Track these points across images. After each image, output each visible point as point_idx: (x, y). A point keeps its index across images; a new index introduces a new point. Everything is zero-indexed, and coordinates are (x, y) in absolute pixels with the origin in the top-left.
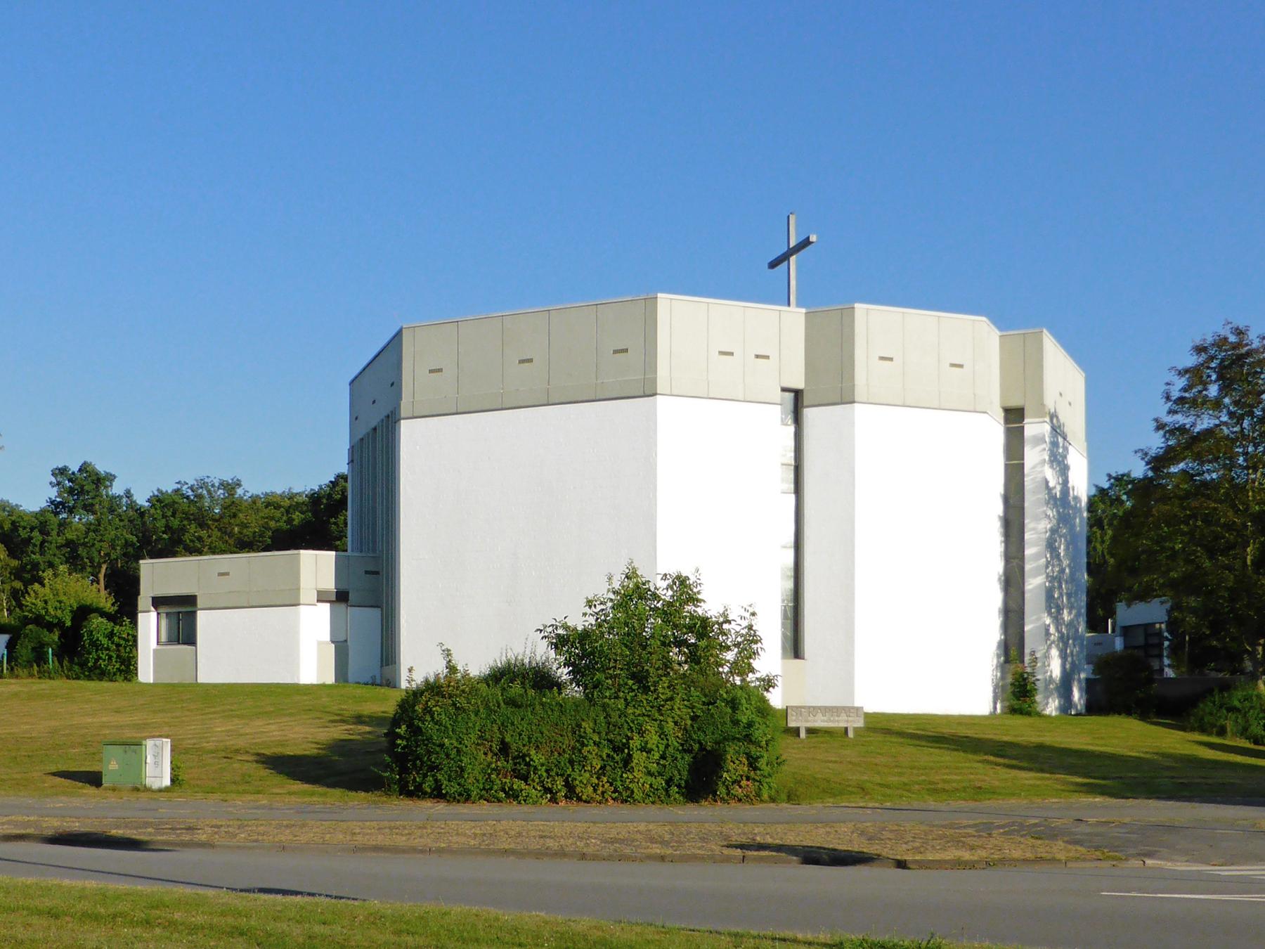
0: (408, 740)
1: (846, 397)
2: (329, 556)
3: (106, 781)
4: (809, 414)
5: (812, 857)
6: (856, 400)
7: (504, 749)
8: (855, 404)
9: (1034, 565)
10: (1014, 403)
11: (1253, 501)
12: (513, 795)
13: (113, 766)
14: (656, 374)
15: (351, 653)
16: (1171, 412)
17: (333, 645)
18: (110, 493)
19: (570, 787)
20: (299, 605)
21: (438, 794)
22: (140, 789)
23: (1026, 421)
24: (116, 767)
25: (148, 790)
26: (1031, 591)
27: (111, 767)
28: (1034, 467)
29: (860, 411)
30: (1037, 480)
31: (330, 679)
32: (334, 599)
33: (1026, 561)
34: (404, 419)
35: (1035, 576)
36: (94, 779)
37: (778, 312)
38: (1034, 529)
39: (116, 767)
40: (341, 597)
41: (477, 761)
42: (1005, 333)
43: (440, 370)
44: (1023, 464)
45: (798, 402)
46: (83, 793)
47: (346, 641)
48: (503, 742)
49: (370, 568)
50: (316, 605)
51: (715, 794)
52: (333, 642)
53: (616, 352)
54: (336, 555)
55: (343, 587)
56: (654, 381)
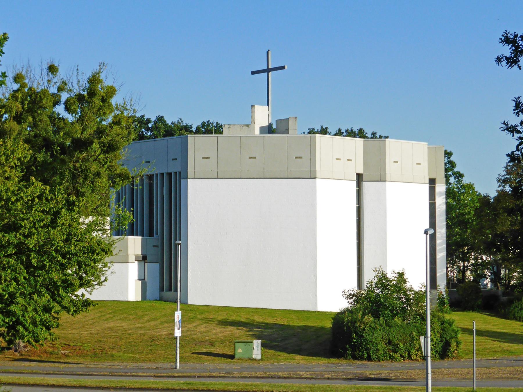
0: (357, 340)
1: (382, 179)
3: (236, 357)
4: (366, 186)
6: (387, 180)
7: (389, 343)
8: (387, 182)
9: (440, 248)
10: (433, 177)
12: (392, 358)
13: (240, 351)
14: (316, 169)
16: (499, 186)
17: (141, 282)
19: (410, 355)
20: (128, 263)
21: (369, 359)
22: (252, 359)
23: (437, 185)
24: (241, 351)
25: (256, 360)
26: (440, 258)
27: (238, 351)
29: (388, 185)
30: (441, 211)
31: (139, 299)
32: (141, 259)
34: (190, 179)
36: (232, 357)
37: (354, 141)
38: (440, 232)
39: (241, 351)
40: (144, 258)
41: (382, 347)
42: (429, 146)
45: (359, 178)
47: (144, 279)
48: (389, 339)
49: (155, 244)
50: (134, 263)
51: (448, 356)
53: (296, 158)
54: (142, 239)
55: (145, 254)
56: (315, 172)
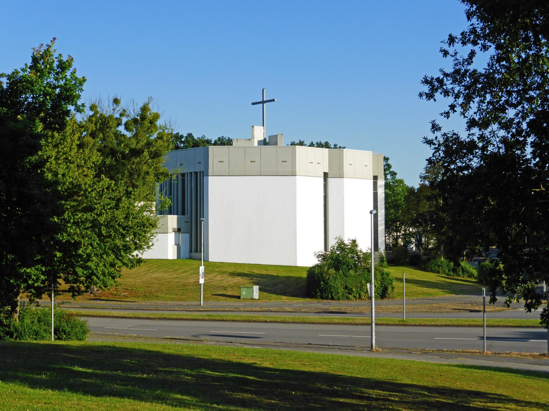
1: (341, 176)
2: (175, 217)
3: (242, 297)
4: (330, 181)
5: (471, 311)
10: (376, 175)
11: (523, 243)
12: (348, 298)
13: (244, 293)
15: (181, 249)
17: (176, 246)
18: (349, 247)
19: (360, 296)
21: (332, 298)
22: (252, 299)
23: (378, 180)
25: (255, 299)
27: (243, 293)
28: (380, 194)
31: (176, 258)
33: (378, 222)
35: (381, 226)
38: (380, 212)
40: (179, 230)
43: (222, 162)
44: (377, 193)
45: (326, 175)
46: (350, 304)
47: (179, 244)
48: (346, 286)
52: (176, 245)
55: (179, 227)
